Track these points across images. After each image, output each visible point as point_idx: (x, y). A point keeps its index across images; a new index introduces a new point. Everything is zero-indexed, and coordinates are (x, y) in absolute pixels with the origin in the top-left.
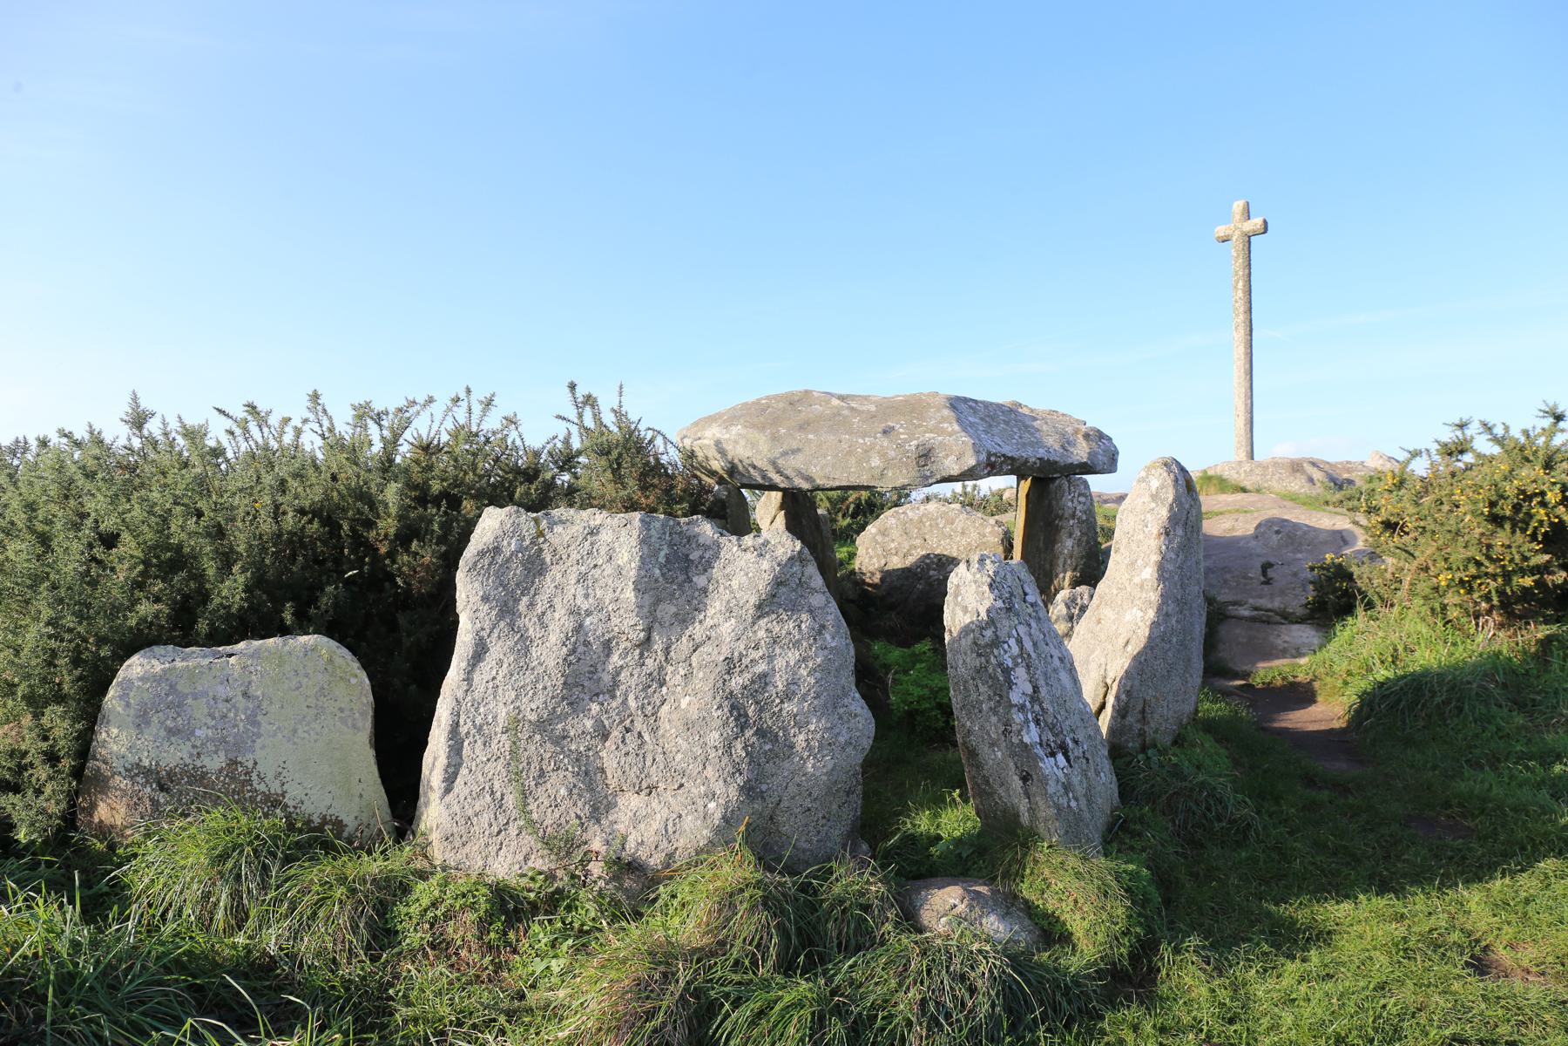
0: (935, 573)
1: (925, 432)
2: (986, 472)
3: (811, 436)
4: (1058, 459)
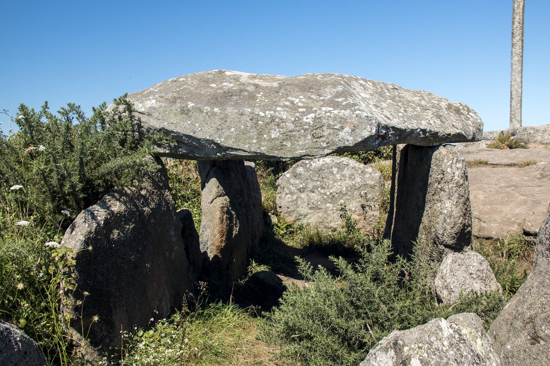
0: (331, 205)
1: (322, 106)
2: (377, 142)
3: (216, 110)
4: (437, 130)
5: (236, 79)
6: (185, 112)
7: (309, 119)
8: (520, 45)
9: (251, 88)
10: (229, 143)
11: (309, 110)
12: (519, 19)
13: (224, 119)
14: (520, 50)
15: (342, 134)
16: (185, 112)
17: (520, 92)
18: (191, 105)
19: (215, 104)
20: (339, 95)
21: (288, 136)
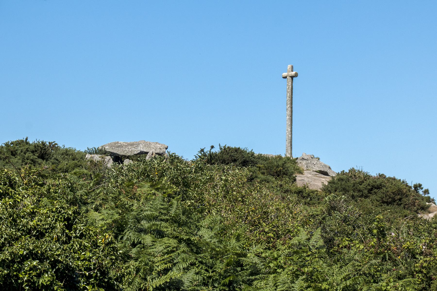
5: (120, 143)
6: (113, 149)
7: (130, 150)
8: (290, 110)
9: (123, 145)
10: (119, 154)
11: (131, 149)
12: (289, 95)
13: (118, 150)
14: (290, 113)
15: (135, 152)
16: (113, 149)
17: (290, 137)
18: (113, 148)
19: (117, 148)
20: (136, 146)
21: (127, 152)
